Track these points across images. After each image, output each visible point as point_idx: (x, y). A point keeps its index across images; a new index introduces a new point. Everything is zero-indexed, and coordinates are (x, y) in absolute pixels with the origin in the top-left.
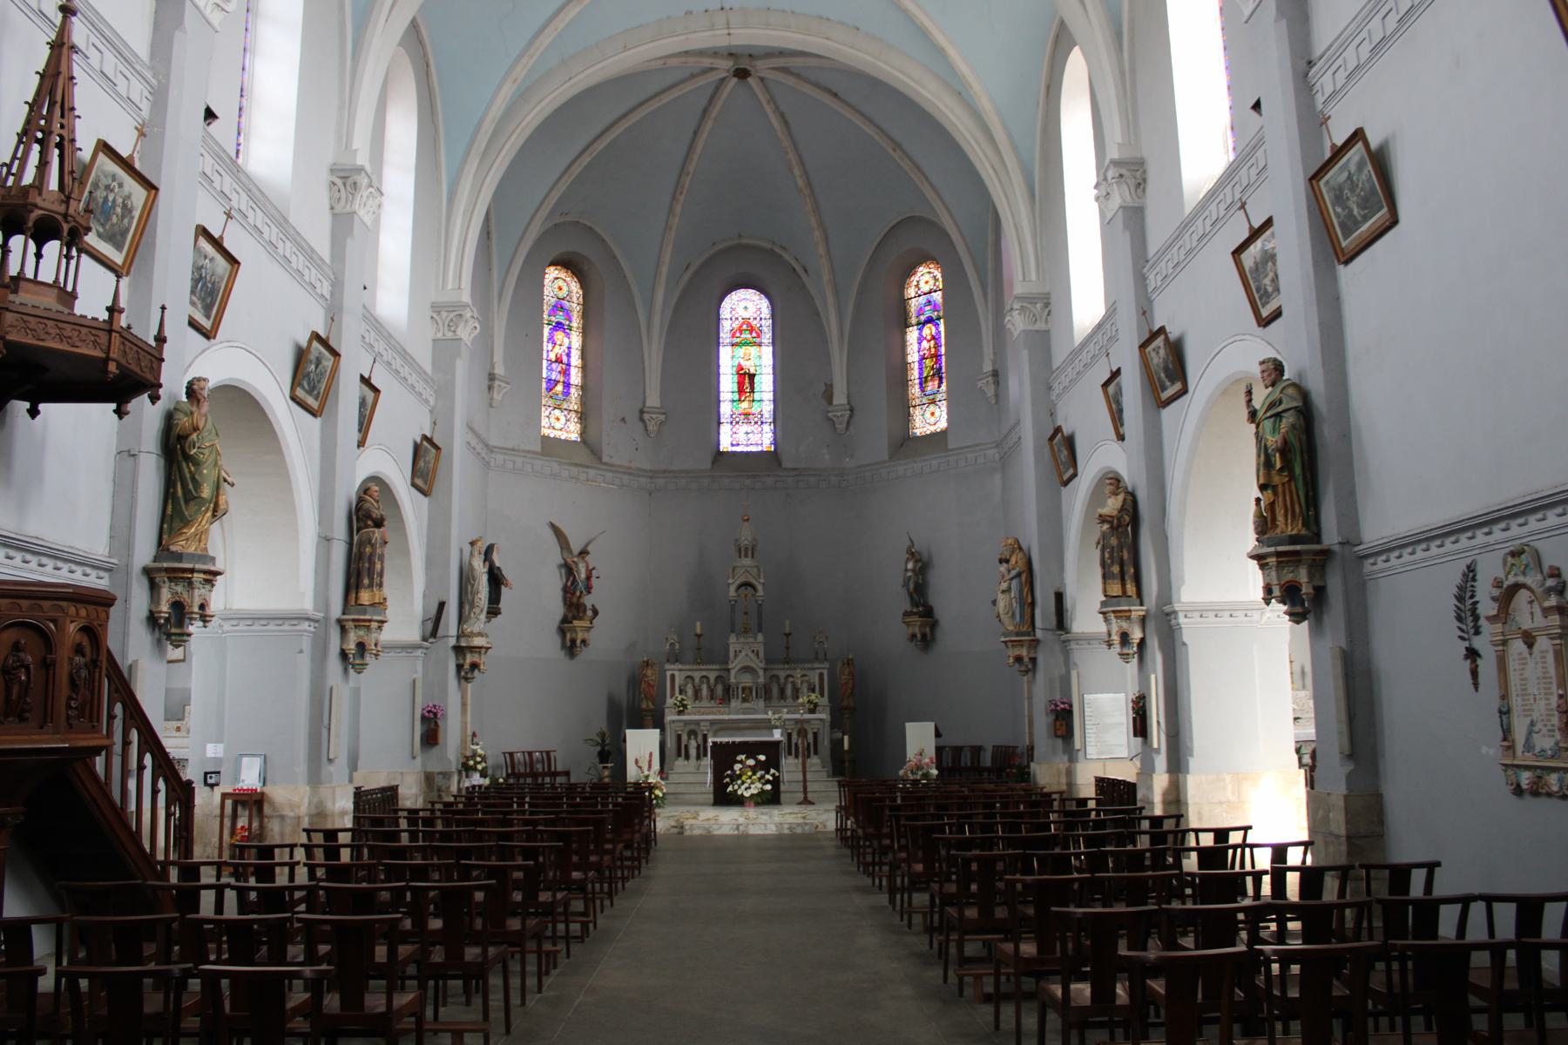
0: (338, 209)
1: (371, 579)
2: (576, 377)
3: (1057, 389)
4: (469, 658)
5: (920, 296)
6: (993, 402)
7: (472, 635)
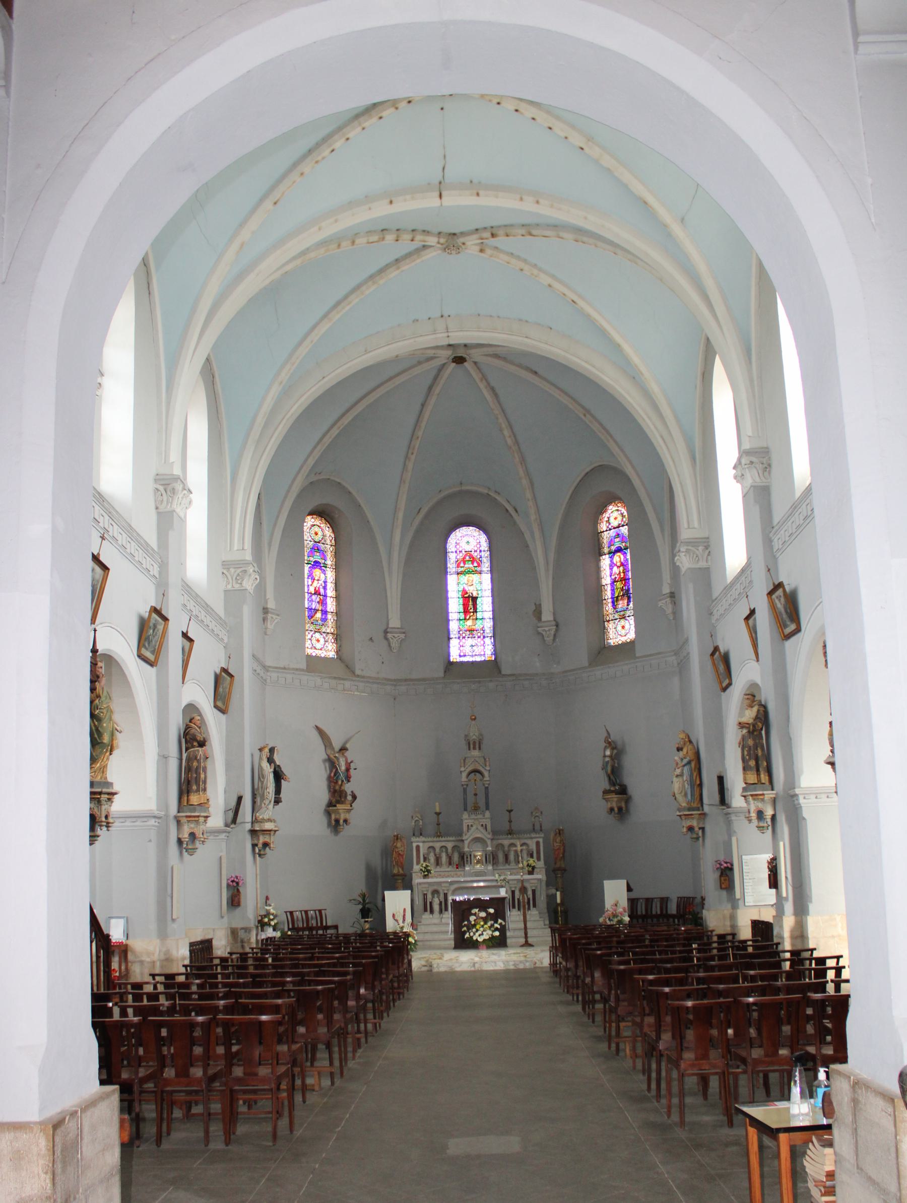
0: (162, 508)
1: (198, 786)
2: (331, 605)
3: (716, 615)
4: (262, 839)
5: (610, 530)
6: (672, 618)
7: (263, 821)
